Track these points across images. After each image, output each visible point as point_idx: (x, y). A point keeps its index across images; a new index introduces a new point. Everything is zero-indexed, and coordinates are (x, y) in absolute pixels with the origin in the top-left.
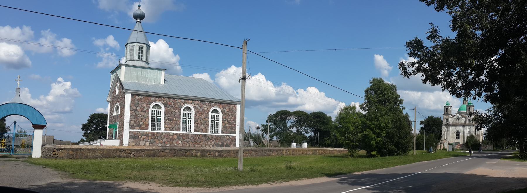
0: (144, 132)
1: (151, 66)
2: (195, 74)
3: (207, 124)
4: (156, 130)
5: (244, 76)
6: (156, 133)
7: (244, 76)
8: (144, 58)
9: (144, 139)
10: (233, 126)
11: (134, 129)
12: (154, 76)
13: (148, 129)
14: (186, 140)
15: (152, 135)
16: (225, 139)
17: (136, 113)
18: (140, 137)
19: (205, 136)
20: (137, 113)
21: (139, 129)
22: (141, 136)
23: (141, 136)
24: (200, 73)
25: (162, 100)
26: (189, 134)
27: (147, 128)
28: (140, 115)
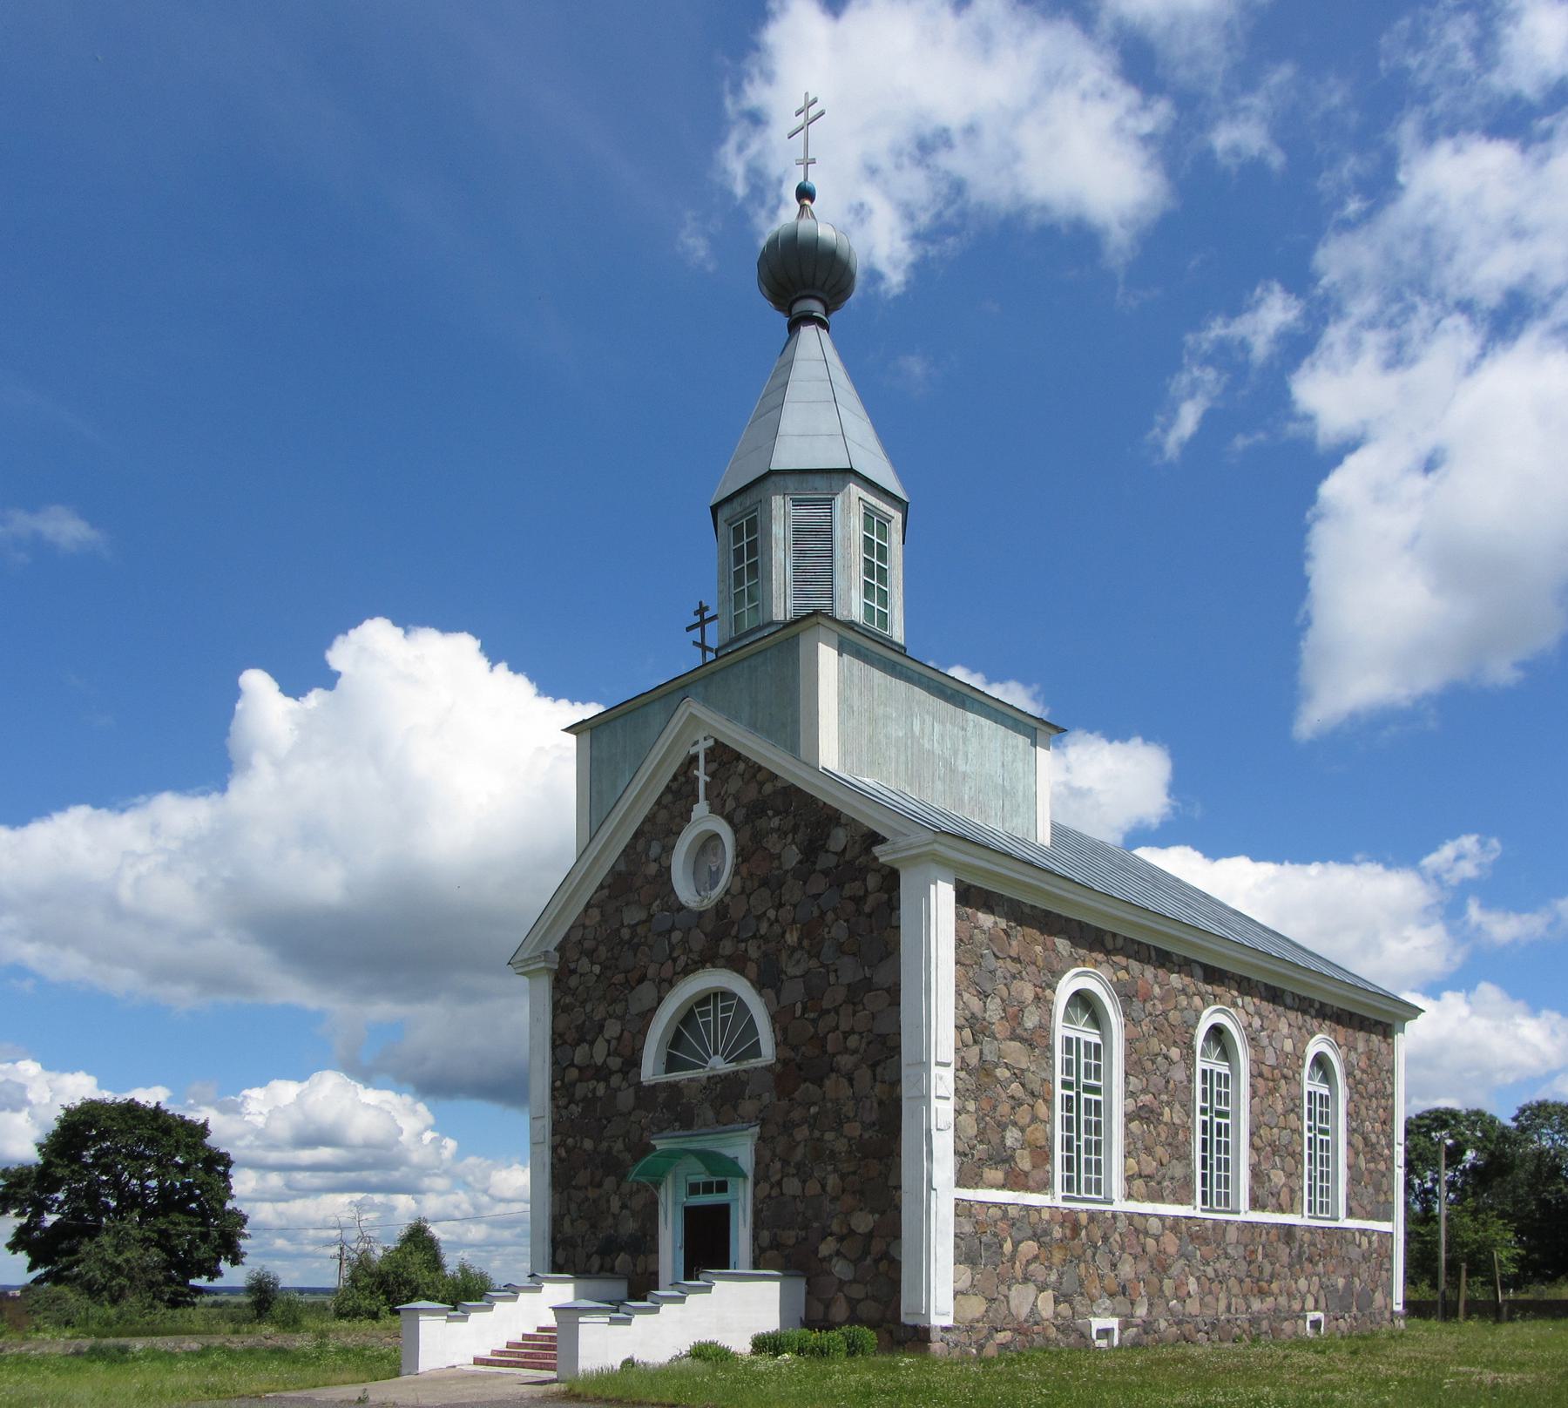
0: (1027, 1207)
1: (907, 654)
2: (465, 646)
3: (1293, 1155)
4: (1079, 1192)
5: (1114, 42)
6: (1084, 1219)
7: (1114, 42)
8: (754, 507)
9: (1028, 1263)
10: (1382, 1166)
11: (976, 1186)
12: (1000, 771)
13: (1045, 1186)
14: (1218, 1265)
15: (1068, 1232)
16: (1355, 1253)
17: (986, 1051)
18: (1008, 1246)
19: (1288, 1231)
20: (989, 1047)
21: (1003, 1187)
22: (1016, 1245)
23: (1016, 1245)
24: (346, 633)
25: (1114, 965)
26: (1227, 1222)
27: (1037, 1175)
28: (1007, 1066)
